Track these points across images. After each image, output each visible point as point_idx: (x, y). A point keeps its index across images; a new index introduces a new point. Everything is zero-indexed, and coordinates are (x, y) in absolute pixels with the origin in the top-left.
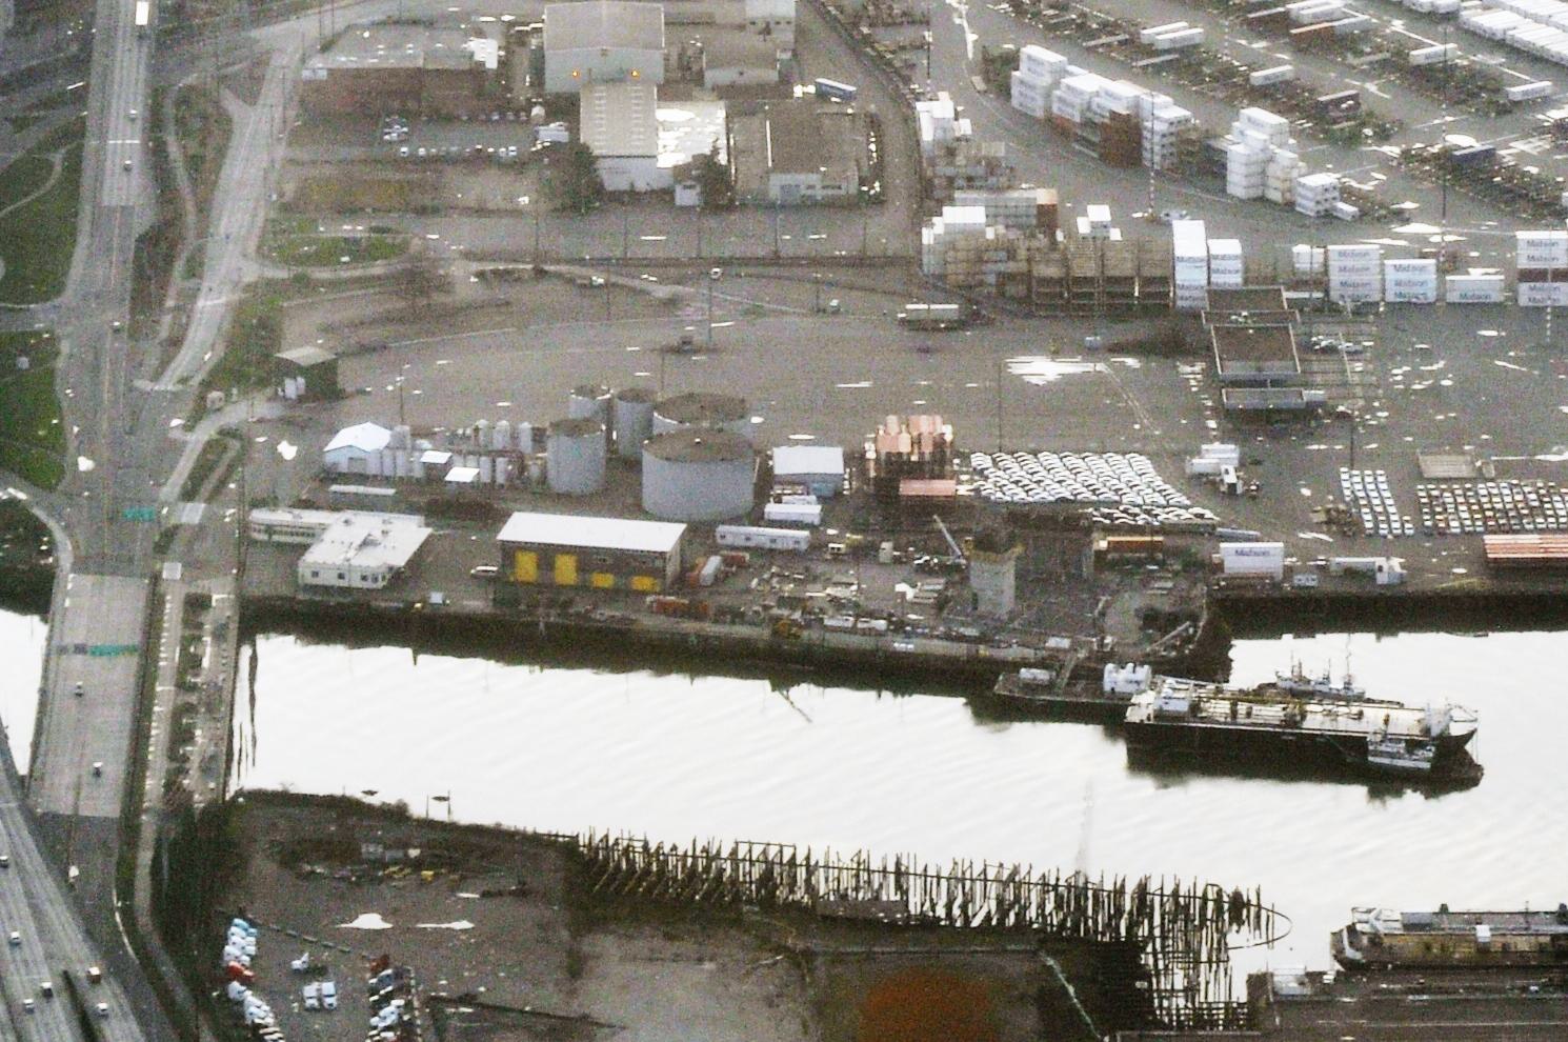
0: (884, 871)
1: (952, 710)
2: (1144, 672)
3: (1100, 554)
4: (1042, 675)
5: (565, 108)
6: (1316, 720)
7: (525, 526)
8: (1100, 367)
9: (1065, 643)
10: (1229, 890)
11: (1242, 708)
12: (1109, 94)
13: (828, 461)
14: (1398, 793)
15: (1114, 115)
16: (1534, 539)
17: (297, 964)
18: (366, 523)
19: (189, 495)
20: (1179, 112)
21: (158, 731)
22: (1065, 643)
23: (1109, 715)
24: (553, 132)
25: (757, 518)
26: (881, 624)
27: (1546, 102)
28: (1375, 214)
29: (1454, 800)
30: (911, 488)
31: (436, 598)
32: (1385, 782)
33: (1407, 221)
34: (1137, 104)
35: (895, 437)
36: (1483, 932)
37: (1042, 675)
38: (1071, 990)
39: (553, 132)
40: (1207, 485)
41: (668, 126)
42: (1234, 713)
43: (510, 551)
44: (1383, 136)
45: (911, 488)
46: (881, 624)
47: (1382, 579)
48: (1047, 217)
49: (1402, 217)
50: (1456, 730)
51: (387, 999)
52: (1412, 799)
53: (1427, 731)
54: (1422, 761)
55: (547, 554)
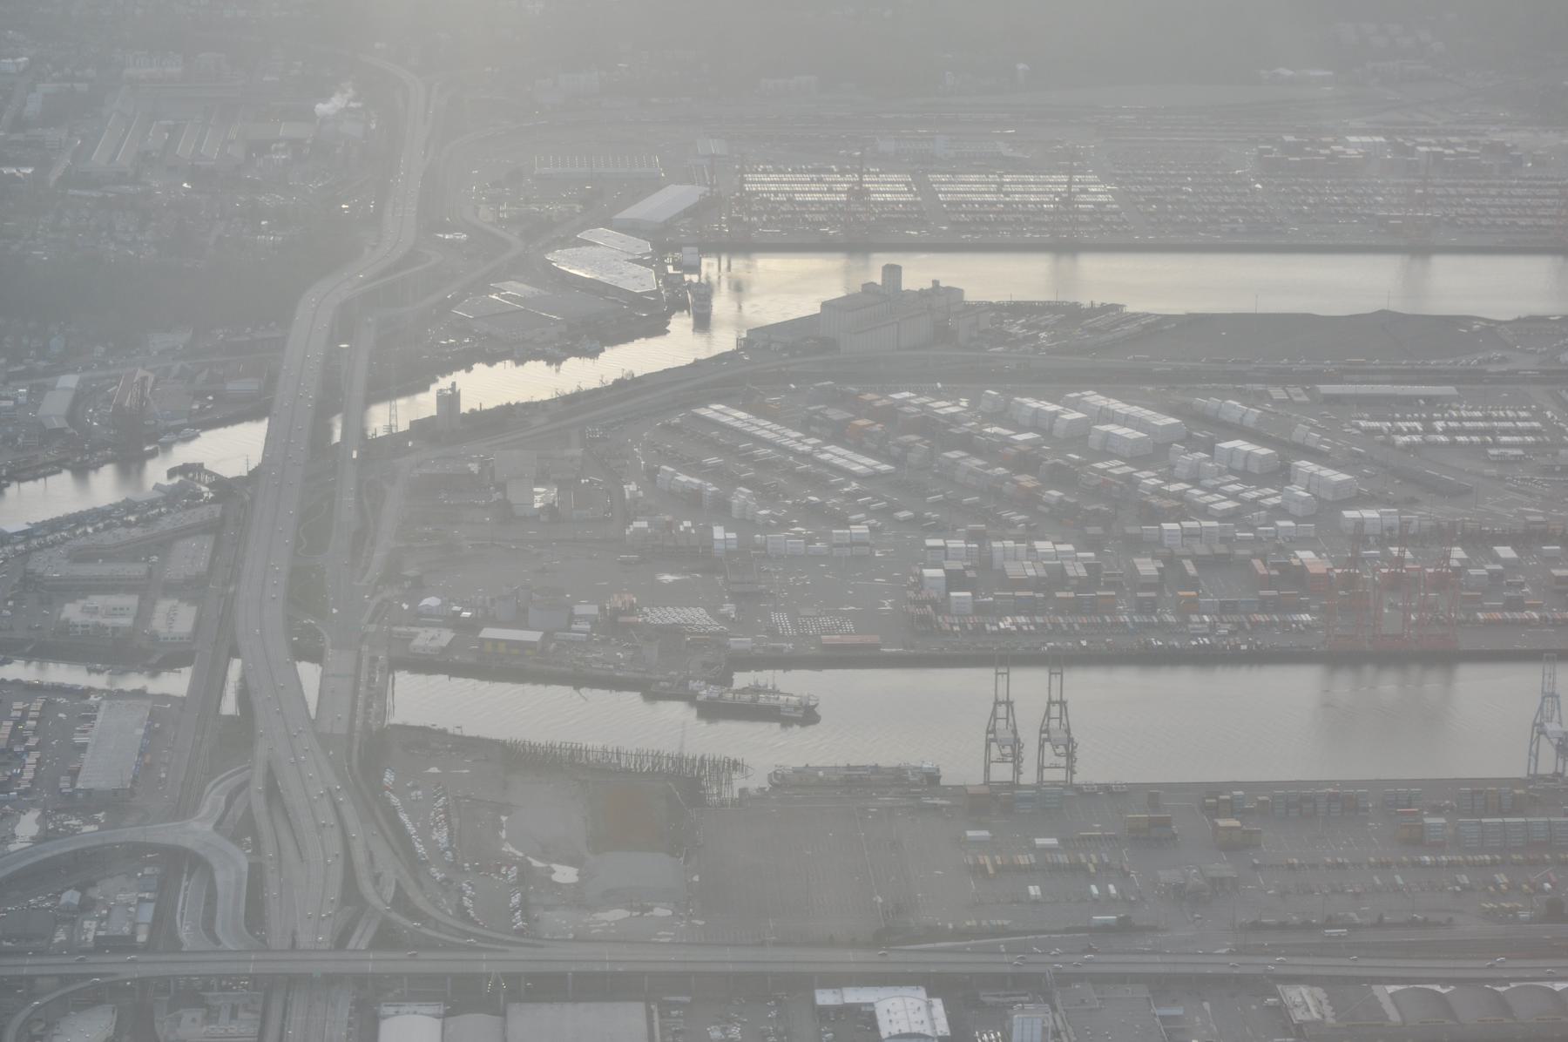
0: (612, 753)
1: (634, 698)
2: (703, 683)
3: (688, 642)
4: (667, 684)
5: (502, 487)
6: (763, 699)
7: (488, 633)
8: (688, 577)
9: (675, 673)
10: (732, 759)
11: (737, 695)
12: (691, 482)
13: (593, 610)
14: (791, 726)
15: (692, 490)
16: (838, 637)
17: (408, 785)
18: (433, 632)
19: (371, 622)
20: (714, 489)
21: (360, 704)
22: (675, 673)
23: (690, 699)
24: (498, 496)
25: (569, 630)
26: (611, 667)
27: (842, 485)
28: (784, 524)
29: (811, 728)
30: (622, 619)
31: (457, 658)
32: (786, 722)
33: (794, 527)
34: (700, 484)
35: (617, 601)
36: (821, 774)
37: (667, 684)
38: (678, 793)
39: (498, 496)
40: (724, 618)
41: (538, 493)
42: (734, 698)
43: (483, 641)
44: (786, 497)
45: (622, 619)
46: (611, 667)
47: (786, 651)
48: (669, 525)
49: (794, 525)
50: (811, 703)
51: (440, 797)
52: (796, 728)
53: (801, 704)
54: (799, 714)
55: (496, 642)
